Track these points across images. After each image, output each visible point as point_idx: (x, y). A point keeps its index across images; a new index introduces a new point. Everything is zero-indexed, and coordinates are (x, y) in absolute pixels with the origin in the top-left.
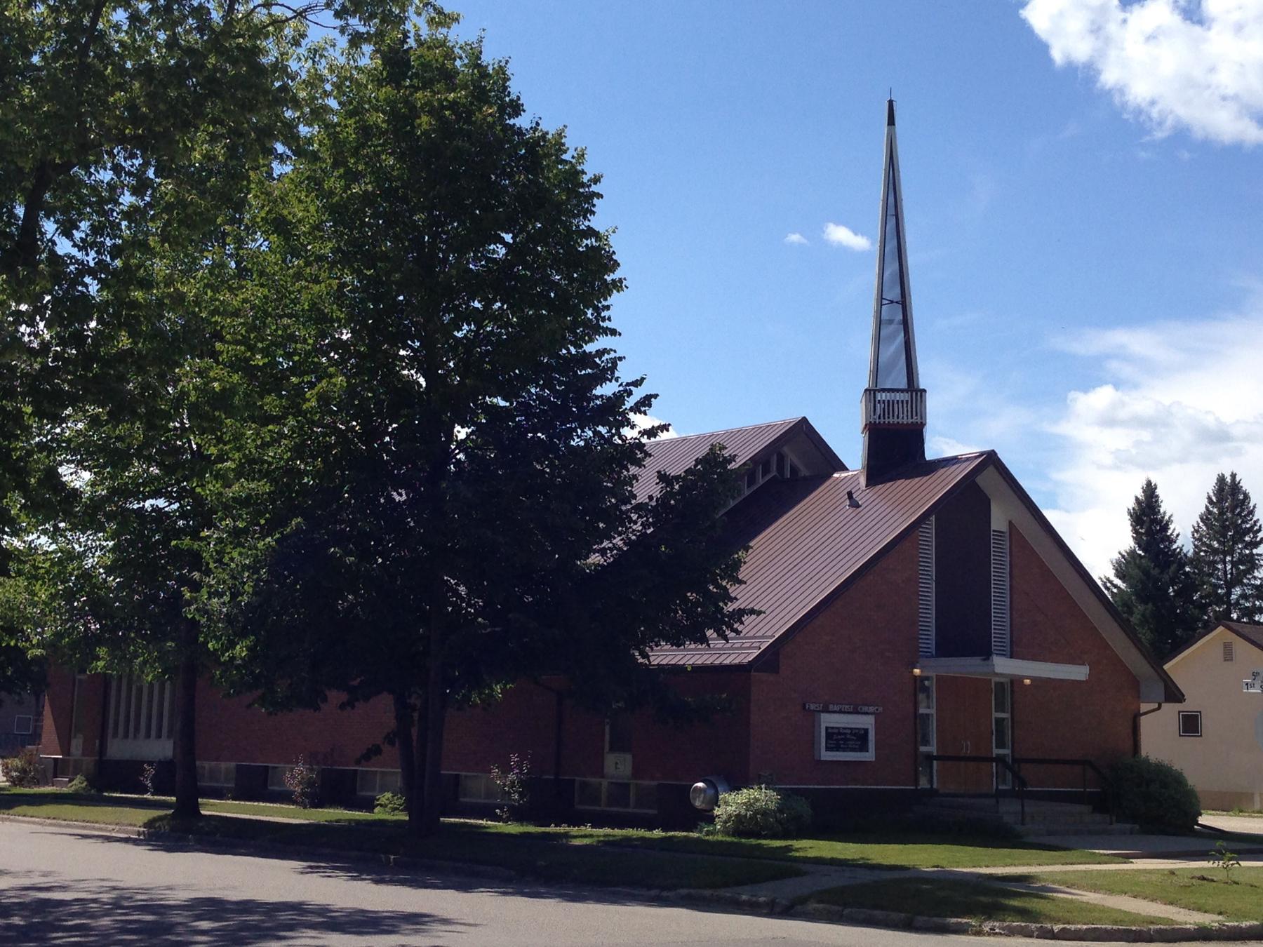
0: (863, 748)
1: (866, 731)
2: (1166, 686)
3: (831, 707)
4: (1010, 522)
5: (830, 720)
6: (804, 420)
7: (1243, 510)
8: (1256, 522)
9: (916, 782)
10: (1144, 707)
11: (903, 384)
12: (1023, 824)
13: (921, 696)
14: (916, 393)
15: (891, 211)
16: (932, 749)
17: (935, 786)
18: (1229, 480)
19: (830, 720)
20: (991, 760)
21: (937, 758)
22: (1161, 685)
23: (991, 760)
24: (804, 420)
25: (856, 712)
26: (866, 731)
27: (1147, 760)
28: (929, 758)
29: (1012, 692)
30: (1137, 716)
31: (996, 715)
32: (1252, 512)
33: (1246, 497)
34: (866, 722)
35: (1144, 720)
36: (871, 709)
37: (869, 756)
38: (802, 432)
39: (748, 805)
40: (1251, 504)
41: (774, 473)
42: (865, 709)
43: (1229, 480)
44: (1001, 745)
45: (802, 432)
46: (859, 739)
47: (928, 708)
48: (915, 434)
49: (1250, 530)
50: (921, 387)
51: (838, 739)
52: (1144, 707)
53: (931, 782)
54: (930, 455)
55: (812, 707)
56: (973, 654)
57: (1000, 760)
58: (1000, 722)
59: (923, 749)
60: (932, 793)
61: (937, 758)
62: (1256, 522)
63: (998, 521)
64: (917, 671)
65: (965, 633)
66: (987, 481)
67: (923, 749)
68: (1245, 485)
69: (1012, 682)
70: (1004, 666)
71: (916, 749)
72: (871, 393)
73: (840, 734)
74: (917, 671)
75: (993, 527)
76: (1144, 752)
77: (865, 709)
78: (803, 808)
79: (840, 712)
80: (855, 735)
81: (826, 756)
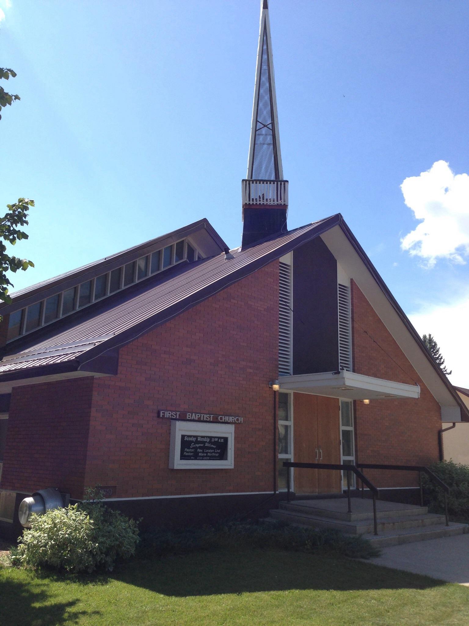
0: (223, 456)
1: (226, 439)
2: (461, 408)
3: (188, 416)
4: (352, 280)
5: (182, 429)
6: (205, 220)
7: (434, 350)
8: (440, 355)
9: (275, 488)
10: (445, 426)
11: (273, 178)
12: (376, 534)
13: (280, 413)
14: (280, 183)
15: (265, 51)
16: (291, 457)
17: (292, 490)
18: (428, 337)
19: (182, 429)
20: (338, 467)
21: (295, 465)
22: (458, 410)
23: (338, 467)
24: (205, 220)
25: (216, 421)
26: (226, 439)
27: (451, 464)
28: (287, 464)
29: (355, 410)
30: (440, 432)
31: (342, 428)
32: (438, 351)
33: (436, 344)
34: (226, 431)
35: (445, 435)
36: (231, 419)
37: (228, 463)
38: (203, 228)
39: (53, 531)
40: (438, 347)
41: (185, 258)
42: (226, 419)
43: (428, 337)
44: (347, 452)
45: (203, 228)
46: (219, 448)
47: (286, 424)
48: (280, 212)
49: (438, 358)
50: (285, 179)
51: (192, 447)
52: (445, 426)
53: (288, 487)
54: (289, 228)
55: (167, 415)
56: (324, 370)
57: (347, 467)
58: (346, 434)
59: (281, 456)
60: (289, 496)
61: (295, 465)
62: (440, 355)
63: (342, 278)
64: (276, 387)
65: (317, 353)
66: (332, 239)
67: (281, 456)
68: (435, 339)
69: (355, 401)
70: (352, 379)
71: (275, 456)
72: (247, 183)
73: (197, 442)
74: (276, 387)
75: (339, 281)
76: (447, 457)
77: (226, 419)
78: (126, 530)
79: (199, 421)
80: (214, 443)
81: (179, 464)
